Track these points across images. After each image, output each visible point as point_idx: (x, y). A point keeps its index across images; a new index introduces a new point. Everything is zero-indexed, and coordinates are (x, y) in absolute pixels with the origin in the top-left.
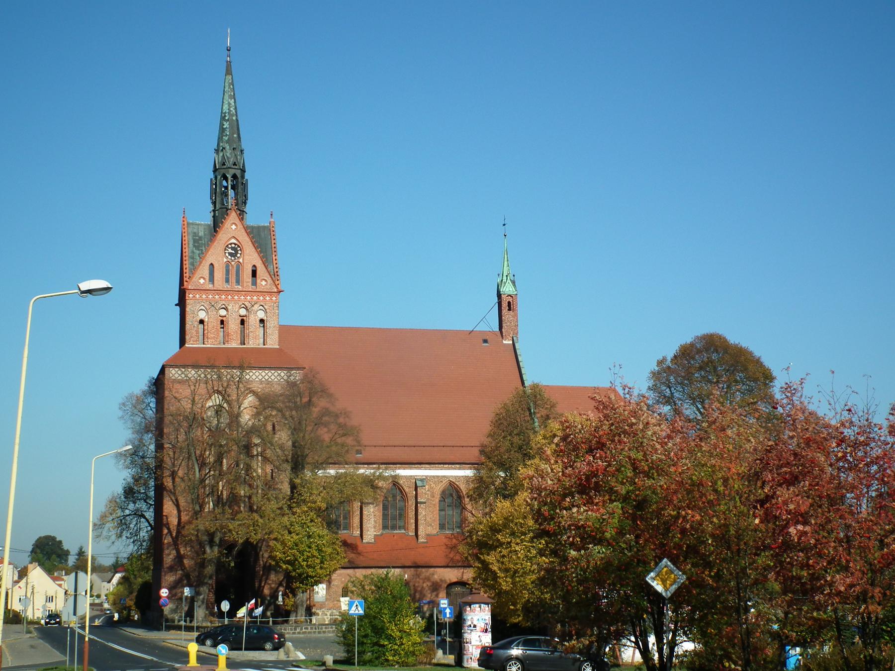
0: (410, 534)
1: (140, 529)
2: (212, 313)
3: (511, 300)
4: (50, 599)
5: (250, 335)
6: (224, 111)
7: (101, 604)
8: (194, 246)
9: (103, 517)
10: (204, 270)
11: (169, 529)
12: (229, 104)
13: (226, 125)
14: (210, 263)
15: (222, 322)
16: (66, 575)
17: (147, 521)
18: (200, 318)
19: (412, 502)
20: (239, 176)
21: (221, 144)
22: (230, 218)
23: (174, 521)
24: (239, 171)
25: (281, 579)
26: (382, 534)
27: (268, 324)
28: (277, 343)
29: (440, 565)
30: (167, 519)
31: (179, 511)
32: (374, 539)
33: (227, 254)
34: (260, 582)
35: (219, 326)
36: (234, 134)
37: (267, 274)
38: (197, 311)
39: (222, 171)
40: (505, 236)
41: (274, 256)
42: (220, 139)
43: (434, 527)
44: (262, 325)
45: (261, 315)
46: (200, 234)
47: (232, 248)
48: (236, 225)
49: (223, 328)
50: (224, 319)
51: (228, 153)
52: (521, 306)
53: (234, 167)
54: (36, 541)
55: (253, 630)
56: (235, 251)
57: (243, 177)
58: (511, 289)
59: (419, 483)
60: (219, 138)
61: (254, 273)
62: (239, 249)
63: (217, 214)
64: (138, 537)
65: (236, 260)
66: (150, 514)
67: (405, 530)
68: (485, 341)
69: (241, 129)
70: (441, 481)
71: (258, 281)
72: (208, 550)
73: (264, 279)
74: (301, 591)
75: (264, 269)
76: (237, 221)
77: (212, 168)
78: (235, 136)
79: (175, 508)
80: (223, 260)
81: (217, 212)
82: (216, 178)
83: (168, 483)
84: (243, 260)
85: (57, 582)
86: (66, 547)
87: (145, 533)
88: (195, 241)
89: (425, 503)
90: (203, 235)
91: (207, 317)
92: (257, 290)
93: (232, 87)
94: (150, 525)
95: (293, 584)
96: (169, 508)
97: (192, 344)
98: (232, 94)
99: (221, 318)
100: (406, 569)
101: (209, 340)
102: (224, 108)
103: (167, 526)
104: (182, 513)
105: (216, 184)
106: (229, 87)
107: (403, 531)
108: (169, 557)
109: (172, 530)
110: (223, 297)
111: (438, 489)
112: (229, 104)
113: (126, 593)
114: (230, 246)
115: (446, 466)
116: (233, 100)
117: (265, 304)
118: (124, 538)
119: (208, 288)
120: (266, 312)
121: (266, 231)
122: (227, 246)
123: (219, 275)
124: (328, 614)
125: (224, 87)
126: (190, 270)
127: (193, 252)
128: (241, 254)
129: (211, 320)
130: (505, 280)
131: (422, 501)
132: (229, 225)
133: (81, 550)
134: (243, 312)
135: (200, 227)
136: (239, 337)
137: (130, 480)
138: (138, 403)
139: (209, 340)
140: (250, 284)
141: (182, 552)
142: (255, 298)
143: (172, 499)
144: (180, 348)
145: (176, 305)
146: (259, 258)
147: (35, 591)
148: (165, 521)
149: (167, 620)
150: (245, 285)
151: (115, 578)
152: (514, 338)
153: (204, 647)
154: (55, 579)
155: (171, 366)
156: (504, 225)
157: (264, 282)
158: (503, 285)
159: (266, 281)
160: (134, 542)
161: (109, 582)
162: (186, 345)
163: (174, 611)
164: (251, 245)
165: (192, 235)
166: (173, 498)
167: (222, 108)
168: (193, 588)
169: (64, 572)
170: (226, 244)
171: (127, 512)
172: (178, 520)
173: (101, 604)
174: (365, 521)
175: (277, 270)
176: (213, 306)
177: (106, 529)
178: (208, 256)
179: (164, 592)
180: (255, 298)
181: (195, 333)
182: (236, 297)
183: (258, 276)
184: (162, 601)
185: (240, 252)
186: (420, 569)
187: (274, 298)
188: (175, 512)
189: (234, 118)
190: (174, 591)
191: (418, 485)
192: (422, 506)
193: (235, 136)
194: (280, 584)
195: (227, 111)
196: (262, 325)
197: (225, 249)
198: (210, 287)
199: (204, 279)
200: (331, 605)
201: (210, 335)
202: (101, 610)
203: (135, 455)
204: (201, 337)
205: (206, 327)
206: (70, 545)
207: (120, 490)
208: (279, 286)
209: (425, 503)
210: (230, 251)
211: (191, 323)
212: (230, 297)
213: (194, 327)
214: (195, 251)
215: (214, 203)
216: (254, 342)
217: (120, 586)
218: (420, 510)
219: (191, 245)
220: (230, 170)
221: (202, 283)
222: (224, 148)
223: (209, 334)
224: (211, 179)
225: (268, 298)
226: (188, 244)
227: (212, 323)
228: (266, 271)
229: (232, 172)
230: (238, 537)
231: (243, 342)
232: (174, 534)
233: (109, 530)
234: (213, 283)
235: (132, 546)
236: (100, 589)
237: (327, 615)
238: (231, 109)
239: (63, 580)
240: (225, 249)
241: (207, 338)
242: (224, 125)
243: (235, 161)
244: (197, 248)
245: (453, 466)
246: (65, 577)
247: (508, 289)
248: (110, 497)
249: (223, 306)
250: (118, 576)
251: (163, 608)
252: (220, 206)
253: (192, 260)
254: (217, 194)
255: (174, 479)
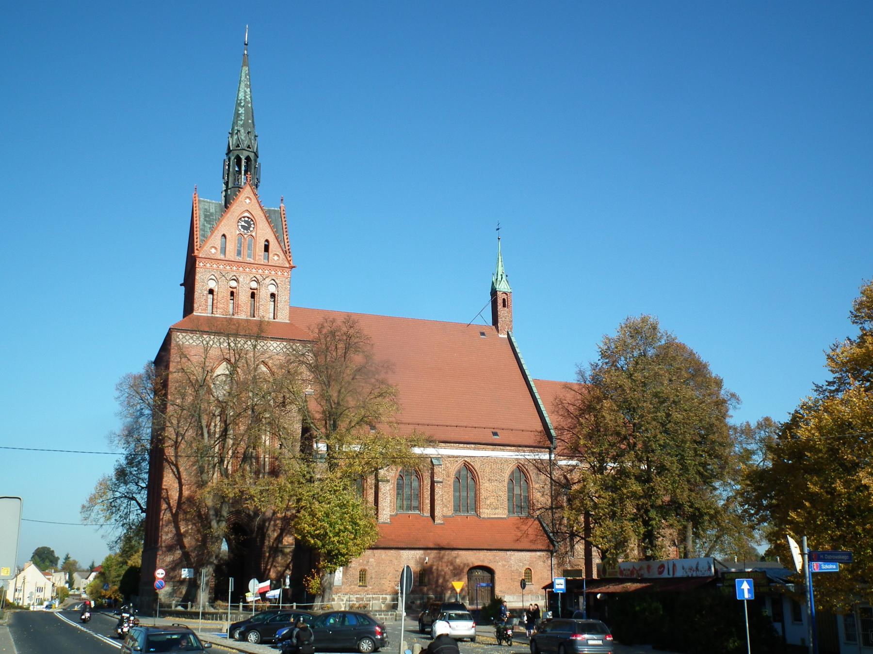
0: (425, 514)
1: (130, 512)
2: (223, 282)
3: (505, 297)
4: (40, 590)
5: (261, 308)
6: (240, 99)
7: (80, 595)
8: (205, 220)
9: (92, 500)
10: (216, 240)
11: (168, 504)
12: (245, 92)
13: (241, 111)
14: (222, 234)
15: (232, 294)
16: (54, 572)
17: (139, 504)
18: (210, 288)
19: (427, 482)
20: (252, 159)
21: (236, 128)
22: (245, 192)
23: (174, 495)
24: (253, 154)
25: (288, 562)
26: (397, 515)
27: (279, 299)
28: (288, 318)
29: (462, 547)
30: (167, 492)
31: (181, 485)
32: (390, 519)
33: (240, 227)
34: (267, 565)
35: (229, 297)
36: (248, 119)
37: (280, 249)
38: (204, 280)
39: (236, 153)
40: (499, 239)
41: (285, 235)
42: (235, 123)
43: (450, 509)
44: (273, 300)
45: (272, 289)
46: (211, 211)
47: (245, 222)
48: (250, 199)
49: (233, 300)
50: (234, 290)
51: (243, 135)
52: (513, 302)
53: (246, 149)
54: (36, 551)
55: (335, 621)
56: (248, 224)
57: (256, 161)
58: (506, 287)
59: (435, 462)
60: (234, 123)
61: (266, 248)
62: (252, 223)
63: (229, 193)
64: (128, 520)
65: (249, 234)
66: (142, 498)
67: (420, 510)
68: (483, 334)
69: (254, 117)
70: (457, 461)
71: (271, 255)
72: (214, 524)
73: (276, 254)
74: (328, 571)
75: (277, 244)
76: (252, 196)
77: (226, 151)
78: (250, 121)
79: (177, 481)
80: (235, 232)
81: (229, 191)
82: (229, 159)
83: (170, 452)
84: (256, 233)
85: (47, 577)
86: (56, 555)
87: (136, 516)
88: (206, 216)
89: (442, 482)
90: (214, 211)
91: (217, 287)
92: (270, 264)
93: (248, 77)
94: (141, 508)
95: (319, 563)
96: (169, 480)
97: (200, 313)
98: (248, 83)
99: (232, 290)
100: (429, 551)
101: (218, 310)
102: (240, 95)
103: (167, 500)
104: (183, 487)
105: (229, 165)
106: (246, 77)
107: (417, 512)
108: (167, 535)
109: (172, 505)
110: (235, 268)
111: (454, 468)
112: (245, 92)
113: (102, 584)
114: (243, 219)
115: (461, 445)
116: (249, 89)
117: (277, 279)
118: (113, 520)
119: (219, 258)
120: (277, 286)
121: (276, 214)
122: (240, 219)
123: (231, 247)
124: (345, 600)
125: (241, 77)
126: (202, 241)
127: (204, 225)
128: (254, 228)
129: (221, 290)
130: (500, 278)
131: (438, 480)
132: (243, 198)
133: (67, 556)
134: (254, 285)
135: (211, 204)
136: (249, 309)
137: (123, 462)
138: (135, 384)
139: (218, 310)
140: (262, 258)
141: (182, 531)
142: (267, 272)
143: (172, 470)
144: (184, 317)
145: (181, 285)
146: (272, 233)
147: (26, 581)
148: (164, 494)
149: (162, 606)
150: (257, 258)
151: (91, 576)
152: (510, 333)
153: (247, 643)
154: (45, 574)
155: (178, 330)
156: (498, 229)
157: (276, 256)
158: (498, 283)
159: (278, 256)
160: (123, 525)
161: (87, 579)
162: (194, 313)
163: (171, 595)
164: (265, 220)
165: (203, 210)
166: (175, 470)
167: (238, 95)
168: (192, 570)
169: (53, 570)
170: (240, 217)
171: (118, 494)
172: (179, 494)
173: (80, 595)
174: (380, 499)
175: (289, 244)
176: (223, 276)
177: (95, 511)
178: (220, 226)
179: (160, 573)
180: (267, 272)
181: (204, 302)
182: (248, 269)
183: (270, 250)
184: (157, 583)
185: (253, 226)
186: (443, 552)
187: (286, 274)
188: (177, 485)
189: (250, 105)
190: (171, 574)
191: (434, 463)
192: (439, 485)
193: (250, 121)
194: (287, 567)
195: (243, 98)
196: (273, 300)
197: (238, 222)
198: (222, 257)
199: (216, 248)
200: (348, 590)
201: (219, 305)
202: (80, 599)
203: (131, 432)
204: (210, 308)
205: (215, 297)
206: (60, 554)
207: (111, 472)
208: (291, 262)
209: (442, 482)
210: (243, 223)
211: (200, 292)
212: (241, 269)
213: (203, 295)
214: (206, 224)
215: (227, 184)
216: (266, 311)
217: (96, 580)
218: (437, 490)
219: (202, 219)
220: (244, 151)
221: (213, 253)
222: (238, 131)
223: (218, 303)
224: (224, 160)
225: (279, 273)
226: (200, 218)
227: (222, 292)
228: (278, 246)
229: (246, 154)
230: (260, 505)
231: (252, 315)
232: (174, 511)
233: (98, 514)
234: (225, 254)
235: (120, 529)
236: (80, 584)
237: (343, 601)
238: (247, 97)
239: (51, 575)
240: (238, 222)
241: (216, 308)
242: (239, 110)
243: (249, 144)
244: (209, 222)
245: (468, 446)
246: (53, 574)
247: (503, 287)
248: (101, 480)
249: (234, 277)
250: (94, 574)
251: (157, 591)
252: (232, 185)
253: (203, 233)
254: (230, 174)
255: (176, 448)
